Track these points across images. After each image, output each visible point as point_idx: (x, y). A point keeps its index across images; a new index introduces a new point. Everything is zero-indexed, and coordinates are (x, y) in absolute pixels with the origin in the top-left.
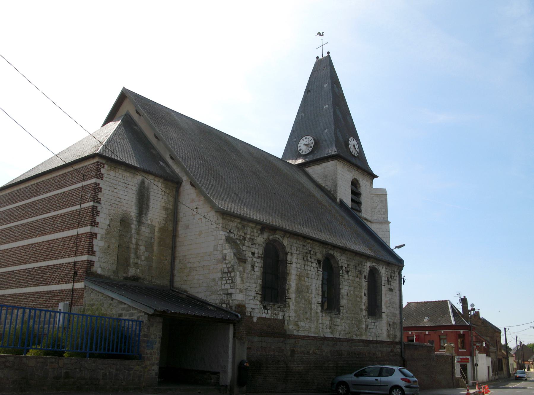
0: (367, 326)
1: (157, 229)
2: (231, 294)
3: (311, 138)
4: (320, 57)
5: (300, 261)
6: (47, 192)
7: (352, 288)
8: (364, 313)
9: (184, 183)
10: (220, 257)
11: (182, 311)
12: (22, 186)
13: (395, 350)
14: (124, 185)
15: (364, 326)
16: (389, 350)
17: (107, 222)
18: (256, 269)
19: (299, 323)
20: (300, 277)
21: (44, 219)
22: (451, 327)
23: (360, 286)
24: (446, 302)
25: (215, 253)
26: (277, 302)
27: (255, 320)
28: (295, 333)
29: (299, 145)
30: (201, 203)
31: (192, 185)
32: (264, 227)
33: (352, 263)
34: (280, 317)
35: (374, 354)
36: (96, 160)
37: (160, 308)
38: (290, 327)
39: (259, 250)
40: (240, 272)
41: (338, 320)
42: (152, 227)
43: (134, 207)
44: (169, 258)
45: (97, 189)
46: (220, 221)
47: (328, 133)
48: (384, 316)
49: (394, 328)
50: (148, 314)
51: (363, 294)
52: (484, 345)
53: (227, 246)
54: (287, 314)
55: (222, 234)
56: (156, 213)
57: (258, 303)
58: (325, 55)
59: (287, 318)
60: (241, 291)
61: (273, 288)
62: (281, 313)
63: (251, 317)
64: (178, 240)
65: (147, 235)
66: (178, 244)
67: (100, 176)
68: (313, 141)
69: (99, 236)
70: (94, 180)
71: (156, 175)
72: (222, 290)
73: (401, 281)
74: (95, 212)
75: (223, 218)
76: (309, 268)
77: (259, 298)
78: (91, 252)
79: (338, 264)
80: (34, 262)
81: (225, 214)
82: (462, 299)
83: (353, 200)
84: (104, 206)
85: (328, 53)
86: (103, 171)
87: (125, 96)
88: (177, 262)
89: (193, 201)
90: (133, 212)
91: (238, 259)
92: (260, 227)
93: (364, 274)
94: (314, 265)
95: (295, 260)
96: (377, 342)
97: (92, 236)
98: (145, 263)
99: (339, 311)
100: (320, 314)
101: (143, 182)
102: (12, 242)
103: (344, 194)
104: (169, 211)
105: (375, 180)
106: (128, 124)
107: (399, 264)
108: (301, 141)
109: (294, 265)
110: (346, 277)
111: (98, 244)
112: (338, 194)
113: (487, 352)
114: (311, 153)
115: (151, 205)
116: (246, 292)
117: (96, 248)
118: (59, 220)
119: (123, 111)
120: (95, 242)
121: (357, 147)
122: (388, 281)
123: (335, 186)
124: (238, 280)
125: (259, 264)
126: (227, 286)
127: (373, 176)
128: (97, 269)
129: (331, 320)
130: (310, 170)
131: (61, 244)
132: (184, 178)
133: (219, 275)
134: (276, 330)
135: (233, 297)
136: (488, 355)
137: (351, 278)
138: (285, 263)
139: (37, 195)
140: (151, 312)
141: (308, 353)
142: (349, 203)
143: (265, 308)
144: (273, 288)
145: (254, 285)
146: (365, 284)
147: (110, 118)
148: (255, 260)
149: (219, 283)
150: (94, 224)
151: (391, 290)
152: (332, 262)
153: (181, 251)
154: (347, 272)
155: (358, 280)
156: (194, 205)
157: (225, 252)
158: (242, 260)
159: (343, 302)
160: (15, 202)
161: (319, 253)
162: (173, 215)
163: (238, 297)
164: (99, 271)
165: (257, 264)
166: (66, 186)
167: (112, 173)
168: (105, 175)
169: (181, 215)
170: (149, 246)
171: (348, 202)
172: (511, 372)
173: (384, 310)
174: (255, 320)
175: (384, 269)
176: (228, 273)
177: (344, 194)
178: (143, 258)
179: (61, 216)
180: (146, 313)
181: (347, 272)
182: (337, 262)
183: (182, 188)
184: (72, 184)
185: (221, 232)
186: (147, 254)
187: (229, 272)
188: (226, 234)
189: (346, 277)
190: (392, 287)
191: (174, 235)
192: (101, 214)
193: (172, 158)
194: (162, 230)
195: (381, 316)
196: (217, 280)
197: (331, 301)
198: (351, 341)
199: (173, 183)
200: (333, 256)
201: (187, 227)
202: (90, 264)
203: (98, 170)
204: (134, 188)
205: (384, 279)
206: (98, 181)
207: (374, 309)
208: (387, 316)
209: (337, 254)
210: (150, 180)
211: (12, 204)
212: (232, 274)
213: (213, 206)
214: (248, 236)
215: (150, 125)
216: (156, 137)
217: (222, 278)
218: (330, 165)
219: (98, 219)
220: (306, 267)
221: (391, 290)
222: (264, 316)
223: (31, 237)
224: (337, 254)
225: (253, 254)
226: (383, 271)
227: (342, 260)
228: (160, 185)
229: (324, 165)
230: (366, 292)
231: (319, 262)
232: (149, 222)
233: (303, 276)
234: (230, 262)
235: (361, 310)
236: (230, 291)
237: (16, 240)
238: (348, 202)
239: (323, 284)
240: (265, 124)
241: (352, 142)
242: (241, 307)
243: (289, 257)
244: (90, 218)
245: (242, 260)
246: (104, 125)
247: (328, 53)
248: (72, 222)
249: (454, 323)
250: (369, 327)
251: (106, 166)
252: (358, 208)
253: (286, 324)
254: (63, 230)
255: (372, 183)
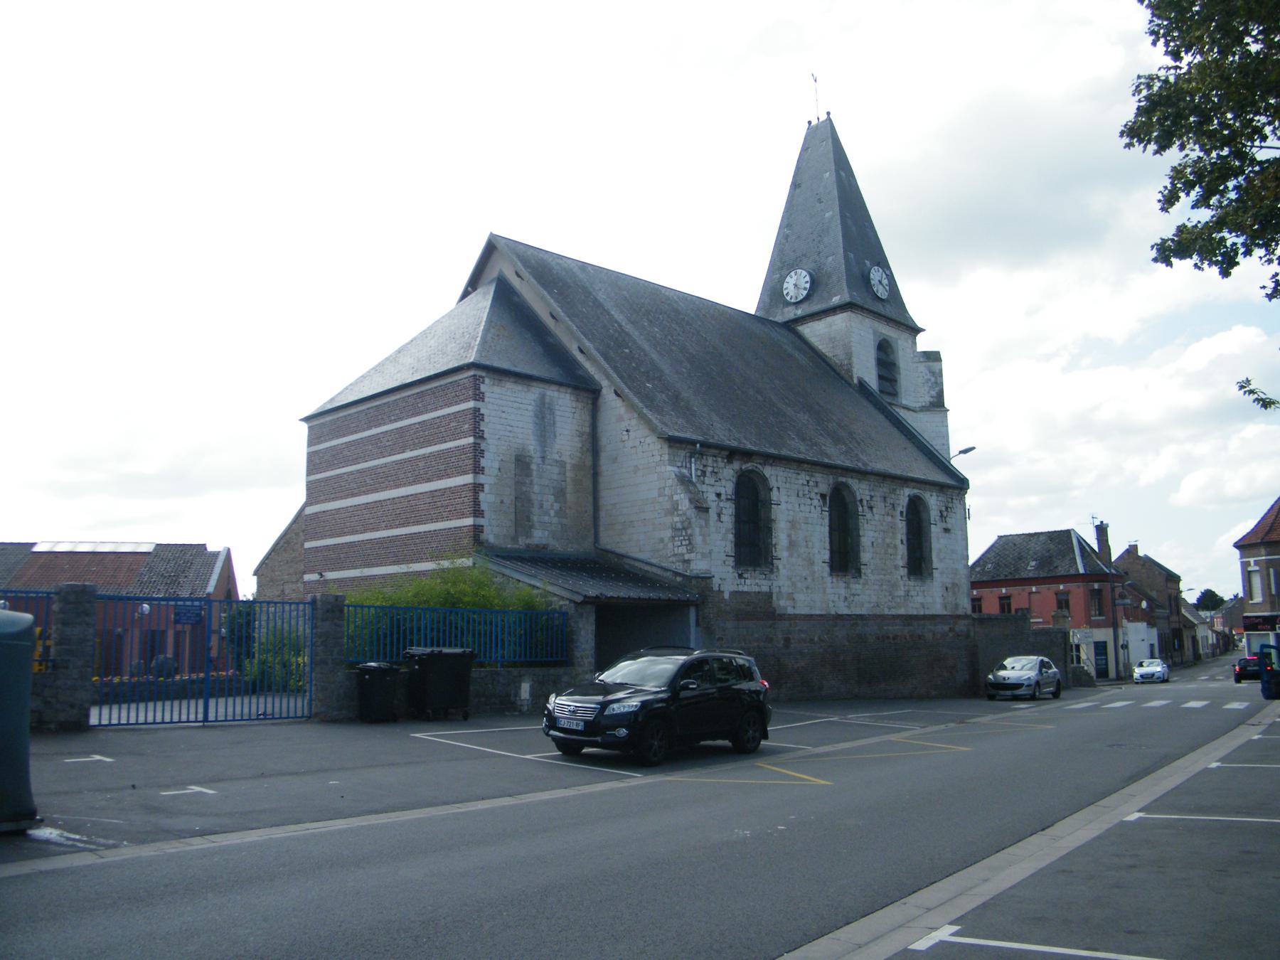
0: (907, 593)
1: (568, 467)
2: (688, 561)
3: (804, 273)
4: (814, 122)
5: (793, 499)
6: (396, 421)
7: (880, 532)
8: (904, 572)
9: (604, 391)
10: (668, 506)
11: (622, 594)
12: (353, 410)
13: (957, 628)
14: (516, 405)
15: (902, 593)
16: (946, 628)
17: (496, 465)
18: (724, 518)
19: (796, 596)
20: (793, 524)
21: (396, 463)
22: (1076, 577)
23: (893, 527)
24: (1068, 532)
25: (661, 499)
26: (759, 566)
27: (726, 596)
28: (790, 611)
29: (785, 285)
30: (634, 422)
31: (618, 395)
32: (733, 454)
33: (878, 494)
34: (765, 589)
35: (920, 637)
36: (471, 373)
37: (592, 592)
38: (783, 604)
39: (728, 488)
40: (701, 527)
41: (858, 586)
42: (562, 464)
43: (532, 437)
44: (590, 508)
45: (477, 416)
46: (666, 450)
47: (835, 260)
48: (936, 574)
49: (954, 593)
50: (575, 602)
51: (898, 542)
52: (1144, 604)
53: (679, 489)
54: (775, 583)
55: (670, 470)
56: (567, 442)
57: (731, 570)
58: (823, 117)
59: (775, 590)
60: (704, 556)
61: (753, 544)
62: (765, 582)
63: (720, 592)
64: (601, 480)
65: (555, 477)
66: (602, 486)
67: (479, 396)
68: (808, 278)
69: (487, 488)
70: (471, 404)
71: (561, 384)
72: (675, 555)
73: (965, 516)
74: (477, 451)
75: (670, 447)
76: (807, 508)
77: (731, 561)
78: (477, 512)
79: (855, 497)
80: (387, 528)
81: (673, 442)
82: (1097, 527)
83: (881, 377)
84: (489, 441)
85: (828, 113)
86: (483, 388)
87: (492, 248)
88: (602, 514)
89: (620, 419)
90: (532, 447)
91: (696, 508)
92: (727, 453)
93: (899, 509)
94: (816, 502)
95: (783, 499)
96: (925, 617)
97: (477, 488)
98: (555, 520)
99: (859, 572)
100: (829, 579)
101: (543, 396)
102: (347, 497)
103: (865, 369)
104: (585, 437)
105: (920, 337)
106: (506, 299)
107: (961, 485)
108: (788, 279)
109: (783, 506)
110: (869, 516)
111: (486, 498)
112: (855, 370)
113: (1149, 618)
114: (807, 298)
115: (559, 431)
116: (711, 555)
117: (484, 506)
118: (421, 464)
119: (492, 273)
120: (482, 496)
121: (885, 282)
122: (942, 516)
123: (849, 356)
124: (698, 540)
125: (729, 509)
126: (683, 550)
127: (915, 330)
128: (489, 536)
129: (847, 587)
130: (808, 330)
131: (428, 500)
132: (605, 383)
133: (669, 533)
134: (761, 610)
135: (693, 566)
136: (1151, 624)
137: (877, 517)
138: (768, 504)
139: (380, 425)
140: (579, 599)
141: (812, 640)
142: (873, 383)
143: (740, 576)
144: (753, 544)
145: (723, 543)
146: (901, 526)
147: (474, 283)
148: (722, 504)
149: (670, 545)
150: (478, 470)
151: (947, 530)
152: (845, 493)
153: (607, 498)
154: (871, 508)
155: (889, 519)
156: (624, 425)
157: (676, 497)
158: (702, 509)
159: (866, 556)
160: (344, 436)
161: (824, 484)
162: (593, 443)
163: (699, 566)
164: (492, 539)
165: (724, 511)
166: (427, 412)
167: (497, 390)
168: (487, 395)
169: (603, 441)
170: (560, 494)
171: (873, 382)
172: (1201, 651)
173: (935, 566)
174: (726, 596)
175: (934, 497)
176: (682, 531)
177: (865, 369)
178: (552, 513)
179: (424, 457)
180: (571, 601)
181: (871, 508)
182: (853, 494)
183: (601, 400)
184: (436, 409)
185: (669, 468)
186: (557, 506)
187: (684, 528)
188: (676, 469)
189: (869, 516)
190: (949, 526)
191: (595, 475)
192: (486, 454)
193: (581, 351)
194: (578, 468)
195: (931, 575)
196: (666, 540)
197: (844, 558)
198: (883, 617)
199: (588, 391)
200: (846, 486)
201: (615, 460)
202: (477, 529)
203: (477, 388)
204: (530, 408)
205: (934, 514)
206: (479, 404)
207: (918, 564)
208: (942, 573)
209: (853, 483)
210: (552, 393)
211: (338, 437)
212: (689, 532)
213: (653, 429)
214: (710, 469)
215: (543, 298)
216: (553, 317)
217: (673, 537)
218: (840, 320)
219: (483, 462)
220: (802, 507)
221: (947, 530)
222: (741, 588)
223: (376, 491)
224: (853, 483)
225: (718, 495)
226: (933, 502)
227: (861, 489)
228: (568, 396)
229: (830, 319)
230: (904, 538)
231: (823, 496)
232: (556, 457)
233: (798, 515)
234: (685, 514)
235: (896, 567)
236: (687, 557)
237: (353, 495)
238: (873, 382)
239: (830, 533)
240: (727, 266)
241: (876, 275)
242: (706, 579)
243: (775, 495)
244: (471, 461)
245: (702, 509)
246: (465, 295)
247: (828, 113)
248: (442, 467)
249: (1081, 571)
250: (912, 593)
251: (487, 380)
252: (891, 390)
253: (774, 598)
254: (429, 480)
255: (915, 343)
